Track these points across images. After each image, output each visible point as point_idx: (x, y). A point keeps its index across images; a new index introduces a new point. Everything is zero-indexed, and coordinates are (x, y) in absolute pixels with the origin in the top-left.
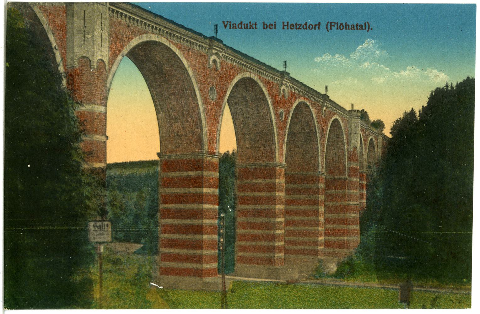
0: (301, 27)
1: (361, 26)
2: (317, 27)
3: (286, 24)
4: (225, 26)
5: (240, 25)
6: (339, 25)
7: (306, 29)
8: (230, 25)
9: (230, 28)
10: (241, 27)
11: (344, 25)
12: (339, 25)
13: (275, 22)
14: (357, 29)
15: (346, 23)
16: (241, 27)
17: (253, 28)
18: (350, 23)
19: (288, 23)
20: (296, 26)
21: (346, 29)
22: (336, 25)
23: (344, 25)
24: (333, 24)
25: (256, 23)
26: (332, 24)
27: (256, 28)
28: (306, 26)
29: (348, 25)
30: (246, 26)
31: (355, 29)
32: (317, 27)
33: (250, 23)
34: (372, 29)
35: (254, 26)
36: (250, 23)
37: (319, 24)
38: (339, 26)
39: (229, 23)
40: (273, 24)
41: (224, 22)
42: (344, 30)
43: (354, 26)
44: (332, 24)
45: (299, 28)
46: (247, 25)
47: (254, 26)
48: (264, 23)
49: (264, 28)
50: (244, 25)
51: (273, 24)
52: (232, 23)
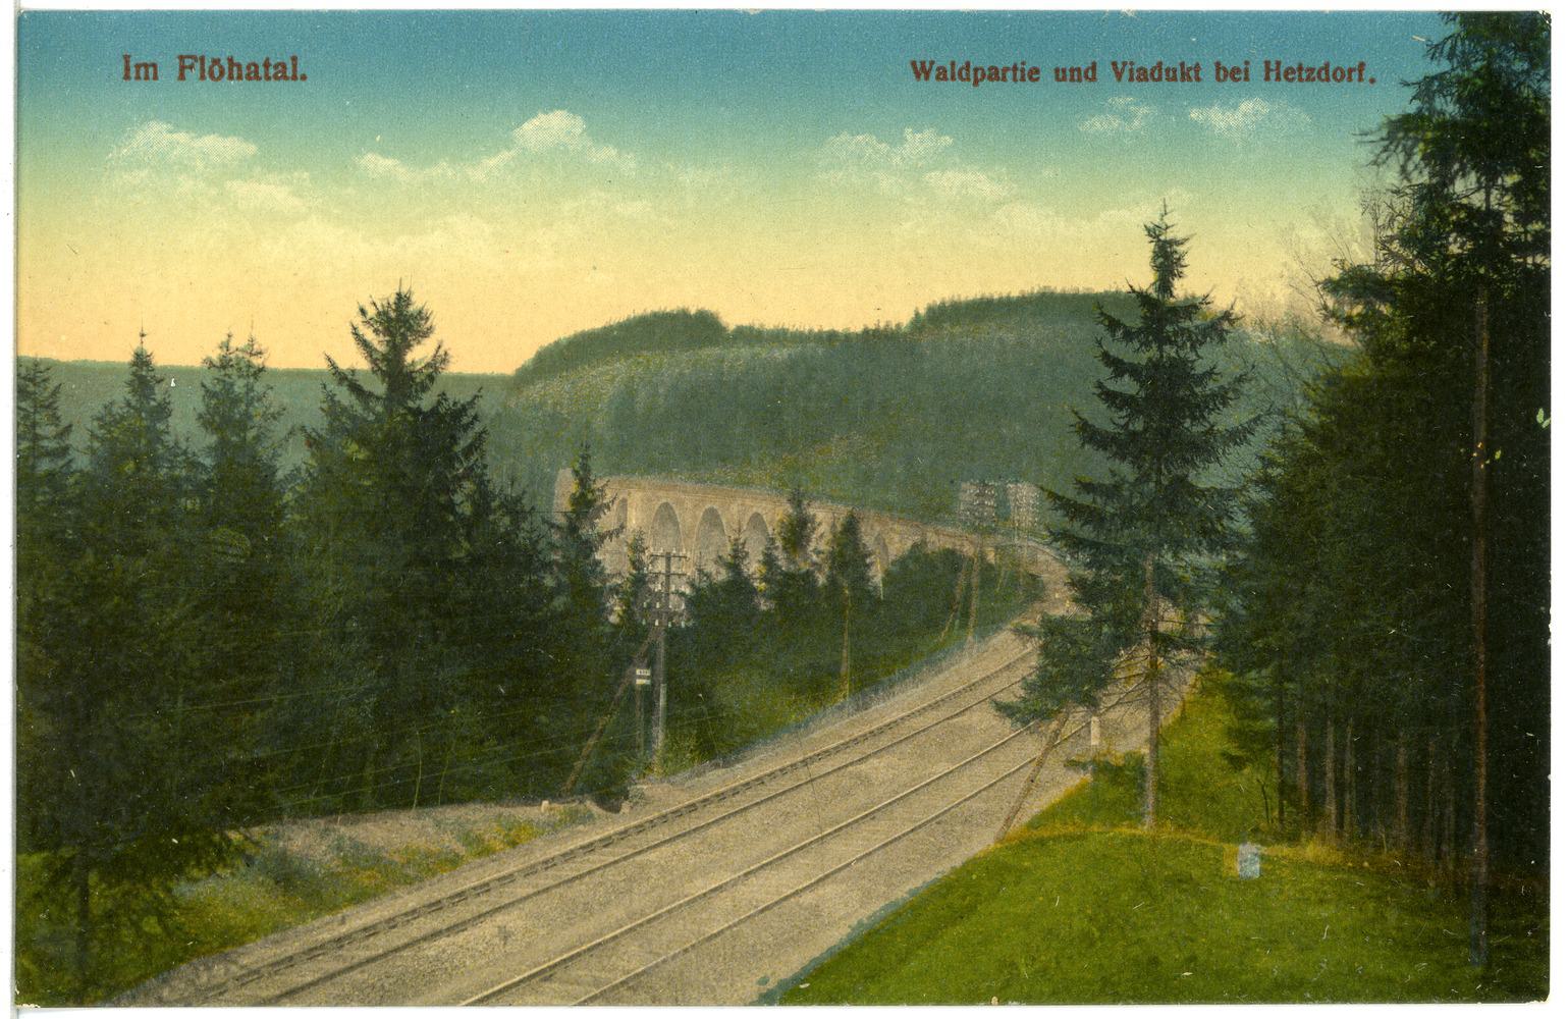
0: (1315, 74)
1: (253, 68)
2: (1355, 75)
3: (1273, 66)
4: (1119, 75)
5: (964, 72)
6: (208, 64)
7: (1328, 80)
8: (1131, 70)
9: (1131, 79)
10: (968, 74)
11: (225, 63)
12: (208, 64)
13: (1247, 63)
14: (268, 78)
15: (230, 60)
16: (968, 74)
17: (1190, 79)
18: (243, 60)
19: (1278, 63)
20: (1300, 75)
21: (231, 78)
22: (197, 65)
23: (225, 63)
24: (188, 62)
25: (1198, 64)
26: (186, 60)
27: (1198, 79)
28: (1325, 74)
29: (239, 66)
30: (1171, 74)
31: (260, 79)
32: (1355, 75)
33: (1182, 64)
34: (1372, 81)
35: (1192, 73)
36: (1182, 64)
37: (1362, 66)
38: (207, 69)
39: (1128, 67)
40: (1242, 67)
41: (1114, 64)
42: (1345, 81)
43: (256, 66)
44: (186, 60)
45: (1308, 79)
46: (1175, 71)
47: (1192, 73)
48: (1218, 64)
49: (1218, 79)
50: (1168, 70)
51: (1242, 67)
52: (1135, 67)
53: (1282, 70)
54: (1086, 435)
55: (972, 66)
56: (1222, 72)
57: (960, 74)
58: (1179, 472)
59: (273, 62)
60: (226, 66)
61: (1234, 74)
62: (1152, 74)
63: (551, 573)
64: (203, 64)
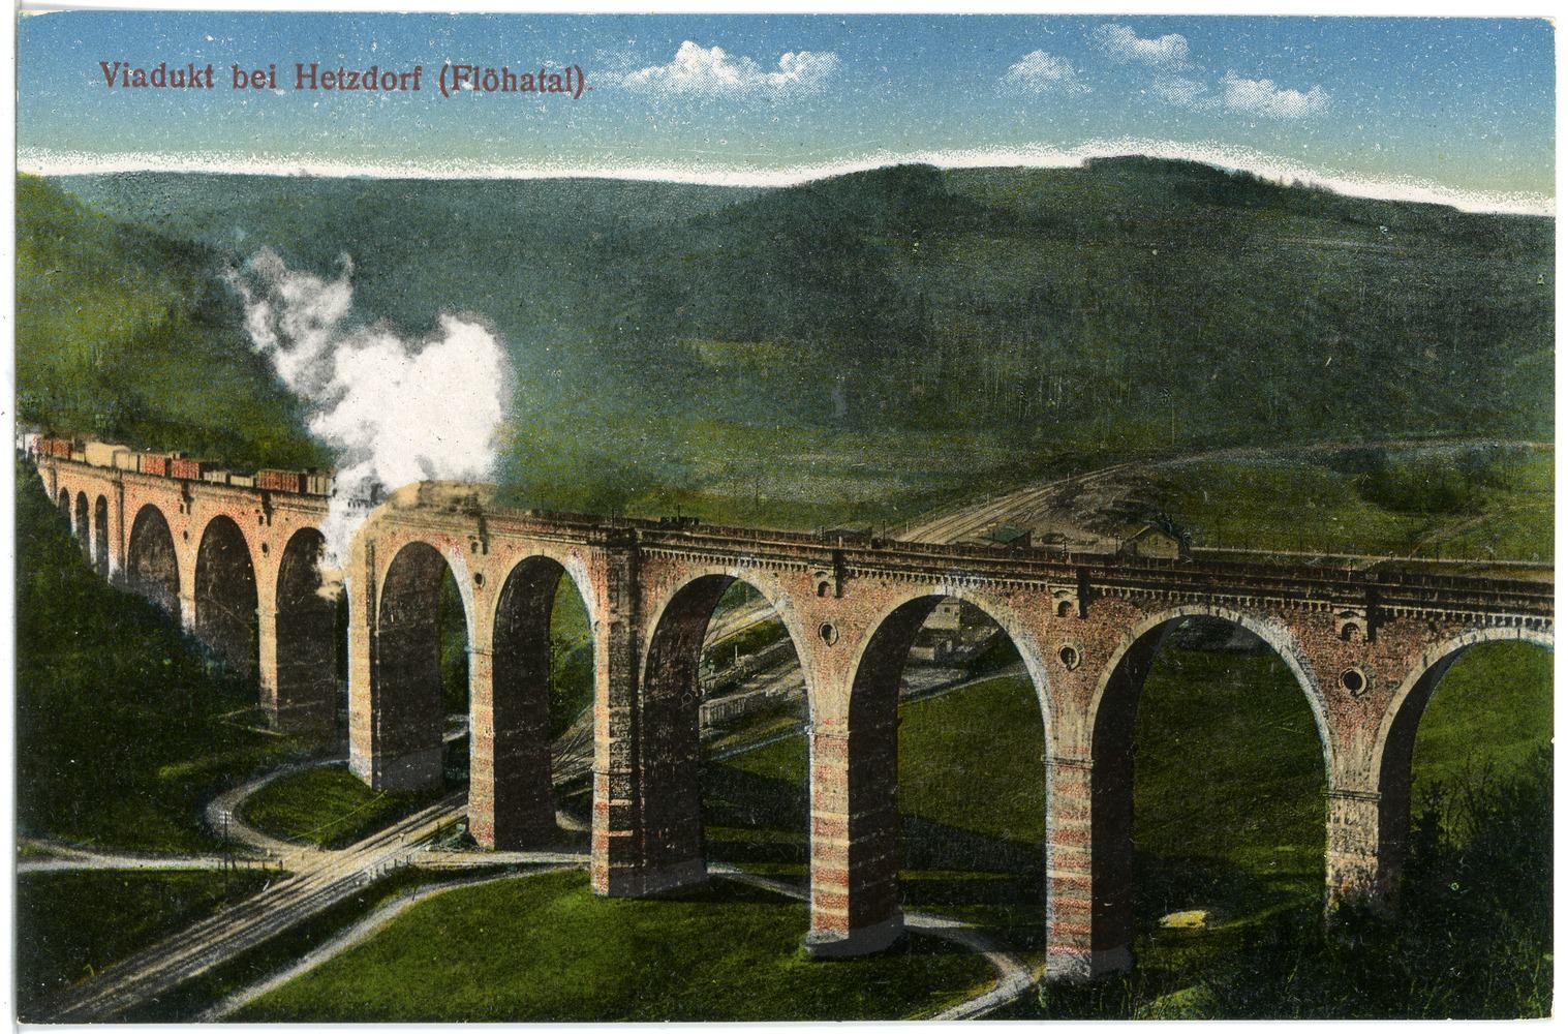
3: (307, 70)
13: (272, 67)
15: (505, 70)
30: (178, 78)
36: (191, 67)
43: (531, 77)
47: (202, 76)
50: (172, 74)
53: (319, 73)
54: (208, 652)
55: (381, 73)
56: (241, 76)
57: (485, 83)
58: (122, 915)
59: (547, 73)
60: (501, 77)
61: (254, 80)
62: (364, 81)
63: (370, 440)
64: (477, 76)
